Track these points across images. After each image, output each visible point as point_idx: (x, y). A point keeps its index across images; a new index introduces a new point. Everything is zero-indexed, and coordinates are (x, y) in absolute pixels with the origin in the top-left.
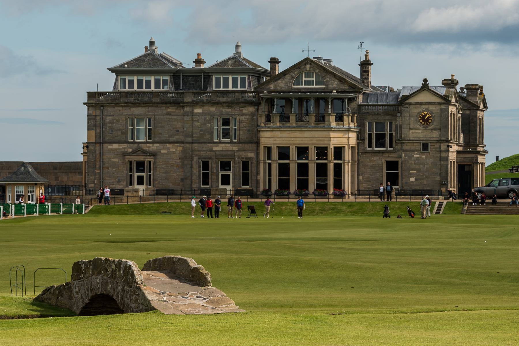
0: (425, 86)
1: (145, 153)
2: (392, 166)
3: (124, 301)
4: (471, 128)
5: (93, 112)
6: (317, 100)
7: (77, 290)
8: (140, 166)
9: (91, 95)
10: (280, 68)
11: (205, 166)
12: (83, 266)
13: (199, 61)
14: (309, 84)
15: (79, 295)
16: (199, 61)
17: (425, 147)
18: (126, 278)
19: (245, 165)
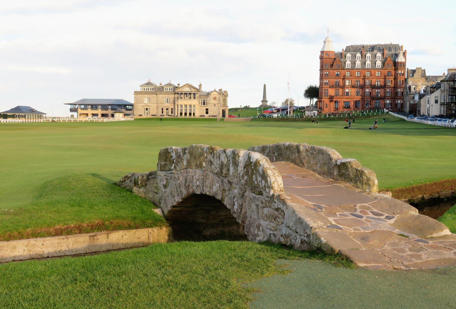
0: (215, 91)
1: (148, 106)
2: (207, 109)
3: (245, 213)
4: (225, 101)
5: (136, 96)
6: (189, 94)
7: (165, 182)
8: (147, 109)
9: (135, 92)
10: (180, 86)
11: (162, 109)
12: (173, 155)
13: (161, 84)
14: (187, 89)
15: (168, 190)
16: (161, 84)
17: (215, 105)
18: (251, 178)
19: (172, 109)
